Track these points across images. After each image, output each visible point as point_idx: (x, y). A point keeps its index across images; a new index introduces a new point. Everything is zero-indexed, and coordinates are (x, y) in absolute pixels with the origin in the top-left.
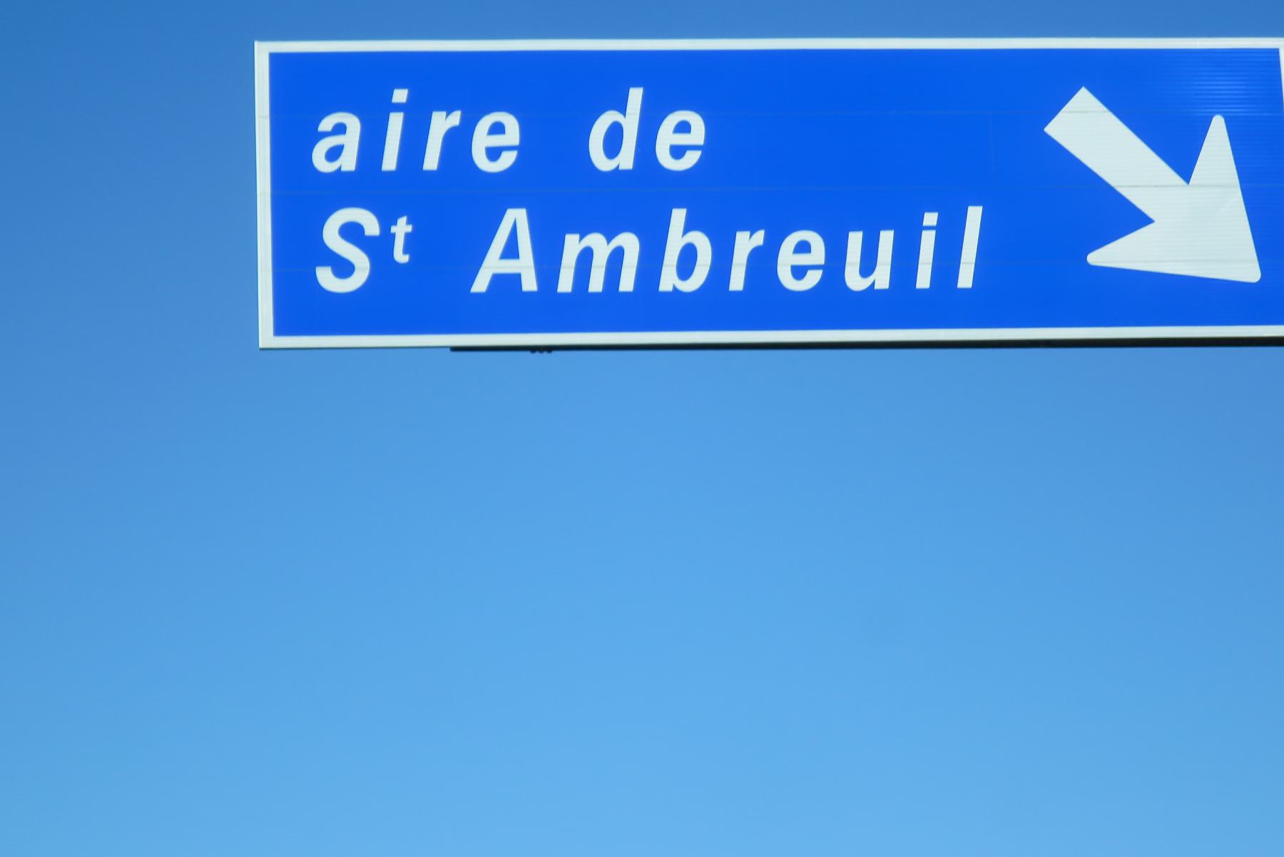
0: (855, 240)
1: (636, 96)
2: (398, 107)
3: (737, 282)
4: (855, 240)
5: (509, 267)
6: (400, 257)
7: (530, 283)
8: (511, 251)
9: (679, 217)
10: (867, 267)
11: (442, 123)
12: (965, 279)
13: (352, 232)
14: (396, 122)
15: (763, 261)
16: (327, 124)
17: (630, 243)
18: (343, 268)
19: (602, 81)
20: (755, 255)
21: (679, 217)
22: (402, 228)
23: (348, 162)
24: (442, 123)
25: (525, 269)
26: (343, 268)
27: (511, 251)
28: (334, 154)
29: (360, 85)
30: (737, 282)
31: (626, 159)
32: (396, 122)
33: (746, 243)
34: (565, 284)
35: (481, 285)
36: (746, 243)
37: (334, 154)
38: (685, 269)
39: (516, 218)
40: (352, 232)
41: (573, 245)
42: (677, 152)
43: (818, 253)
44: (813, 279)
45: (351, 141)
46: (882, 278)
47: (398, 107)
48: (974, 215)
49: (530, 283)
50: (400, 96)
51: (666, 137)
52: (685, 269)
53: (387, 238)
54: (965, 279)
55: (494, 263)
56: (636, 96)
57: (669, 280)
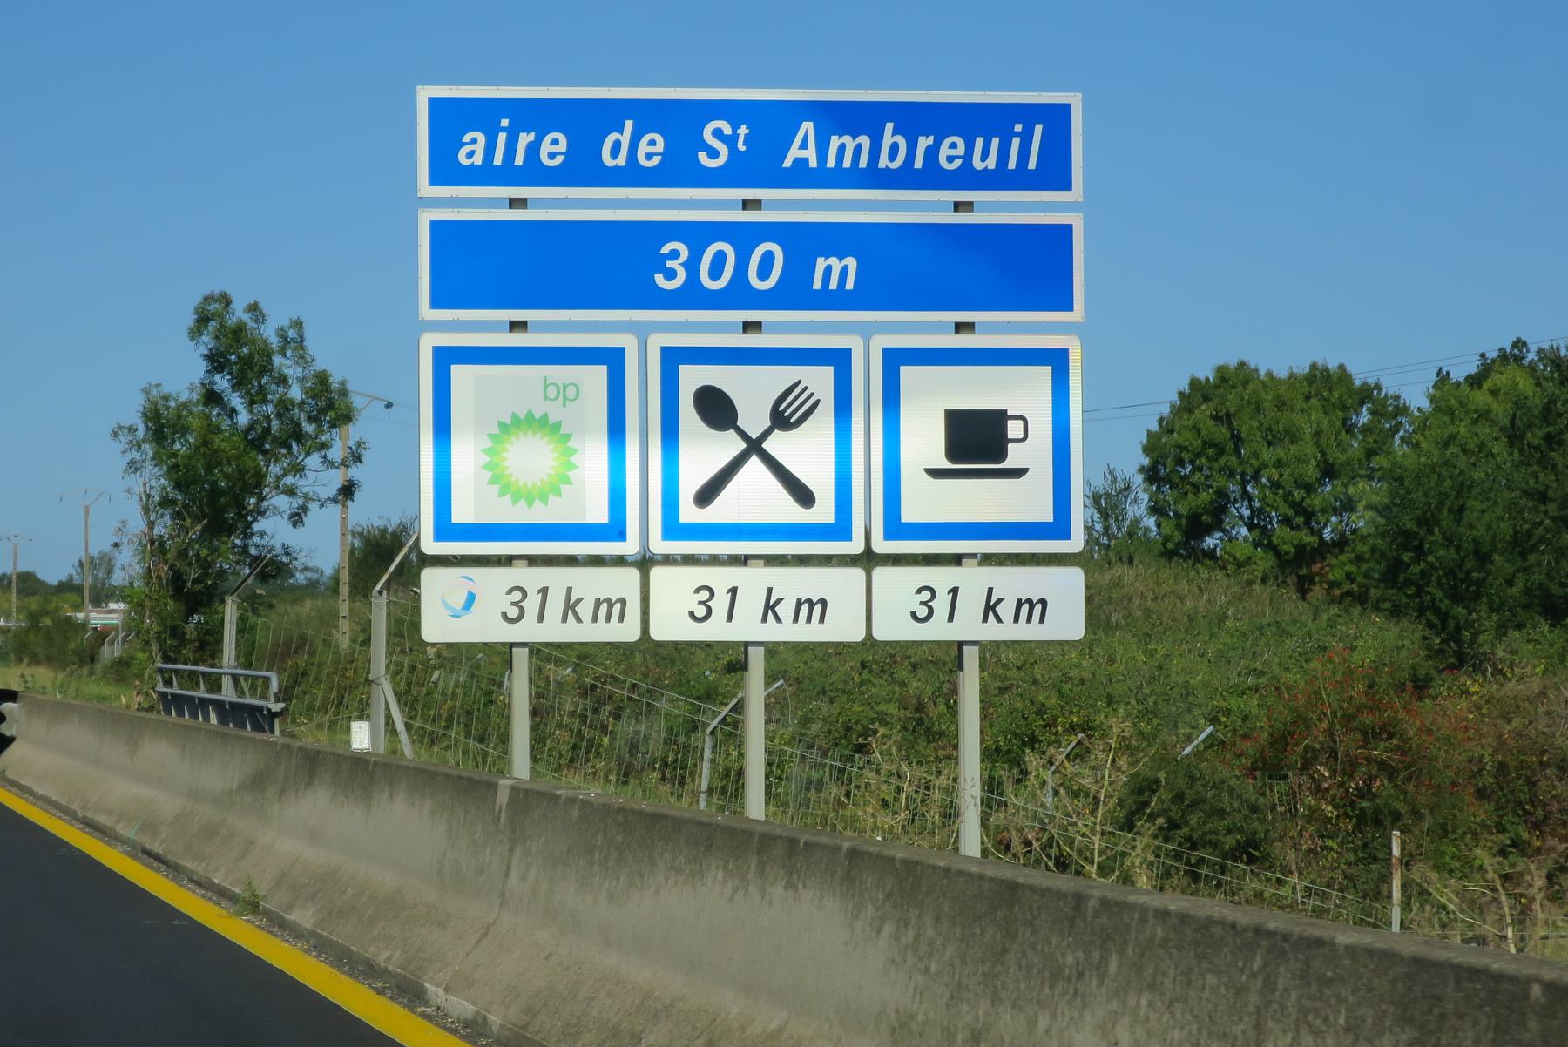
0: (979, 142)
1: (629, 124)
2: (504, 130)
3: (918, 164)
4: (979, 142)
5: (803, 154)
6: (741, 147)
7: (813, 163)
8: (804, 145)
9: (889, 127)
10: (984, 157)
11: (525, 139)
12: (1032, 165)
13: (718, 134)
14: (502, 137)
15: (932, 152)
16: (467, 138)
17: (865, 141)
18: (714, 154)
19: (609, 114)
20: (928, 149)
21: (889, 127)
22: (743, 131)
23: (478, 160)
24: (525, 139)
25: (811, 154)
26: (714, 154)
27: (804, 145)
28: (470, 155)
29: (483, 114)
30: (918, 164)
31: (621, 161)
32: (502, 137)
33: (924, 142)
34: (831, 163)
35: (787, 163)
36: (924, 142)
37: (470, 155)
38: (893, 154)
39: (808, 127)
40: (718, 134)
41: (835, 142)
42: (649, 156)
43: (961, 150)
44: (957, 163)
45: (480, 148)
46: (991, 163)
47: (504, 130)
48: (1039, 128)
49: (813, 163)
50: (505, 123)
51: (643, 148)
52: (893, 154)
53: (735, 136)
54: (1032, 165)
55: (794, 152)
56: (629, 124)
57: (884, 162)
